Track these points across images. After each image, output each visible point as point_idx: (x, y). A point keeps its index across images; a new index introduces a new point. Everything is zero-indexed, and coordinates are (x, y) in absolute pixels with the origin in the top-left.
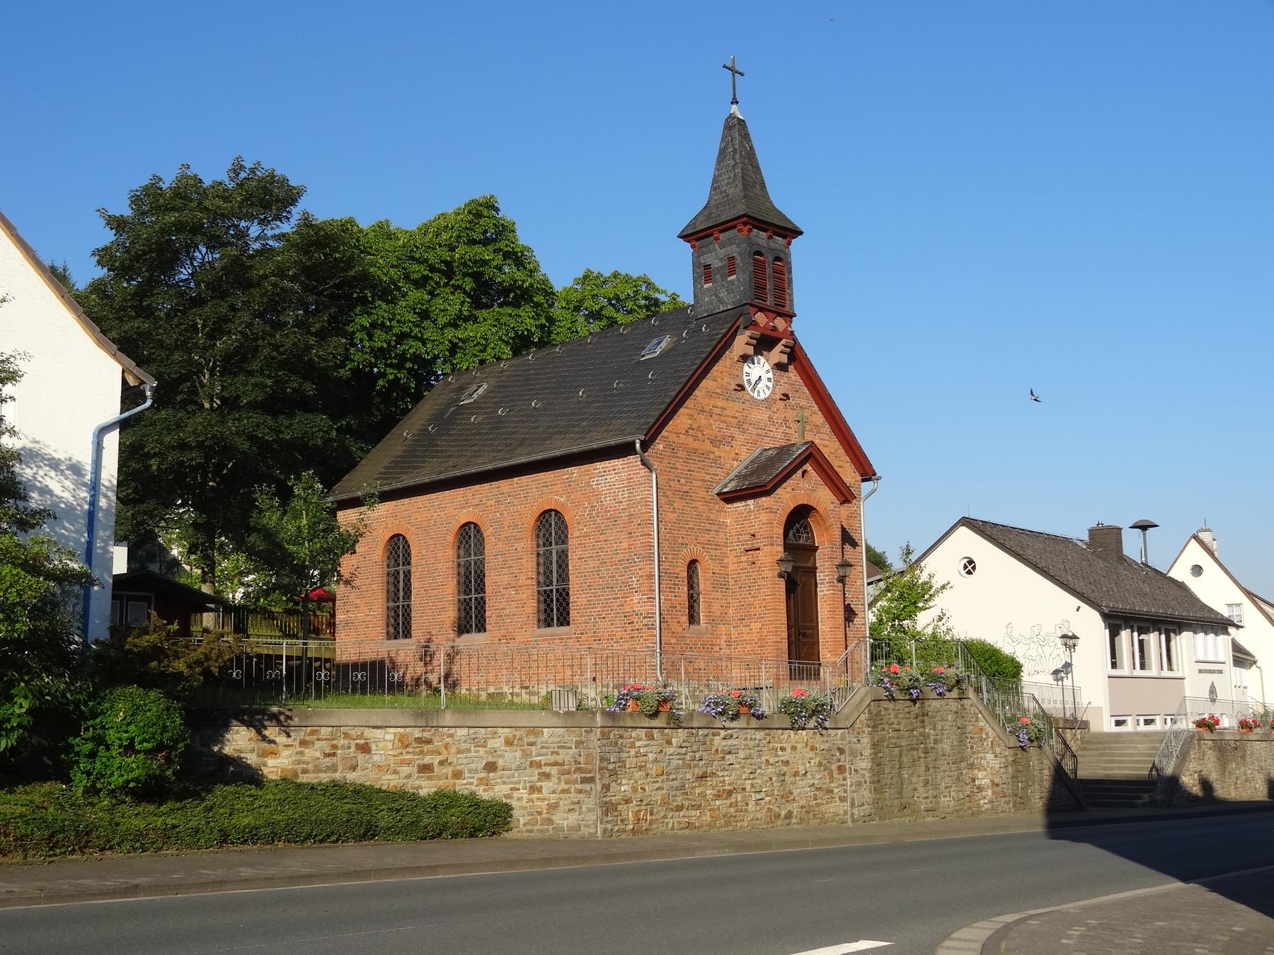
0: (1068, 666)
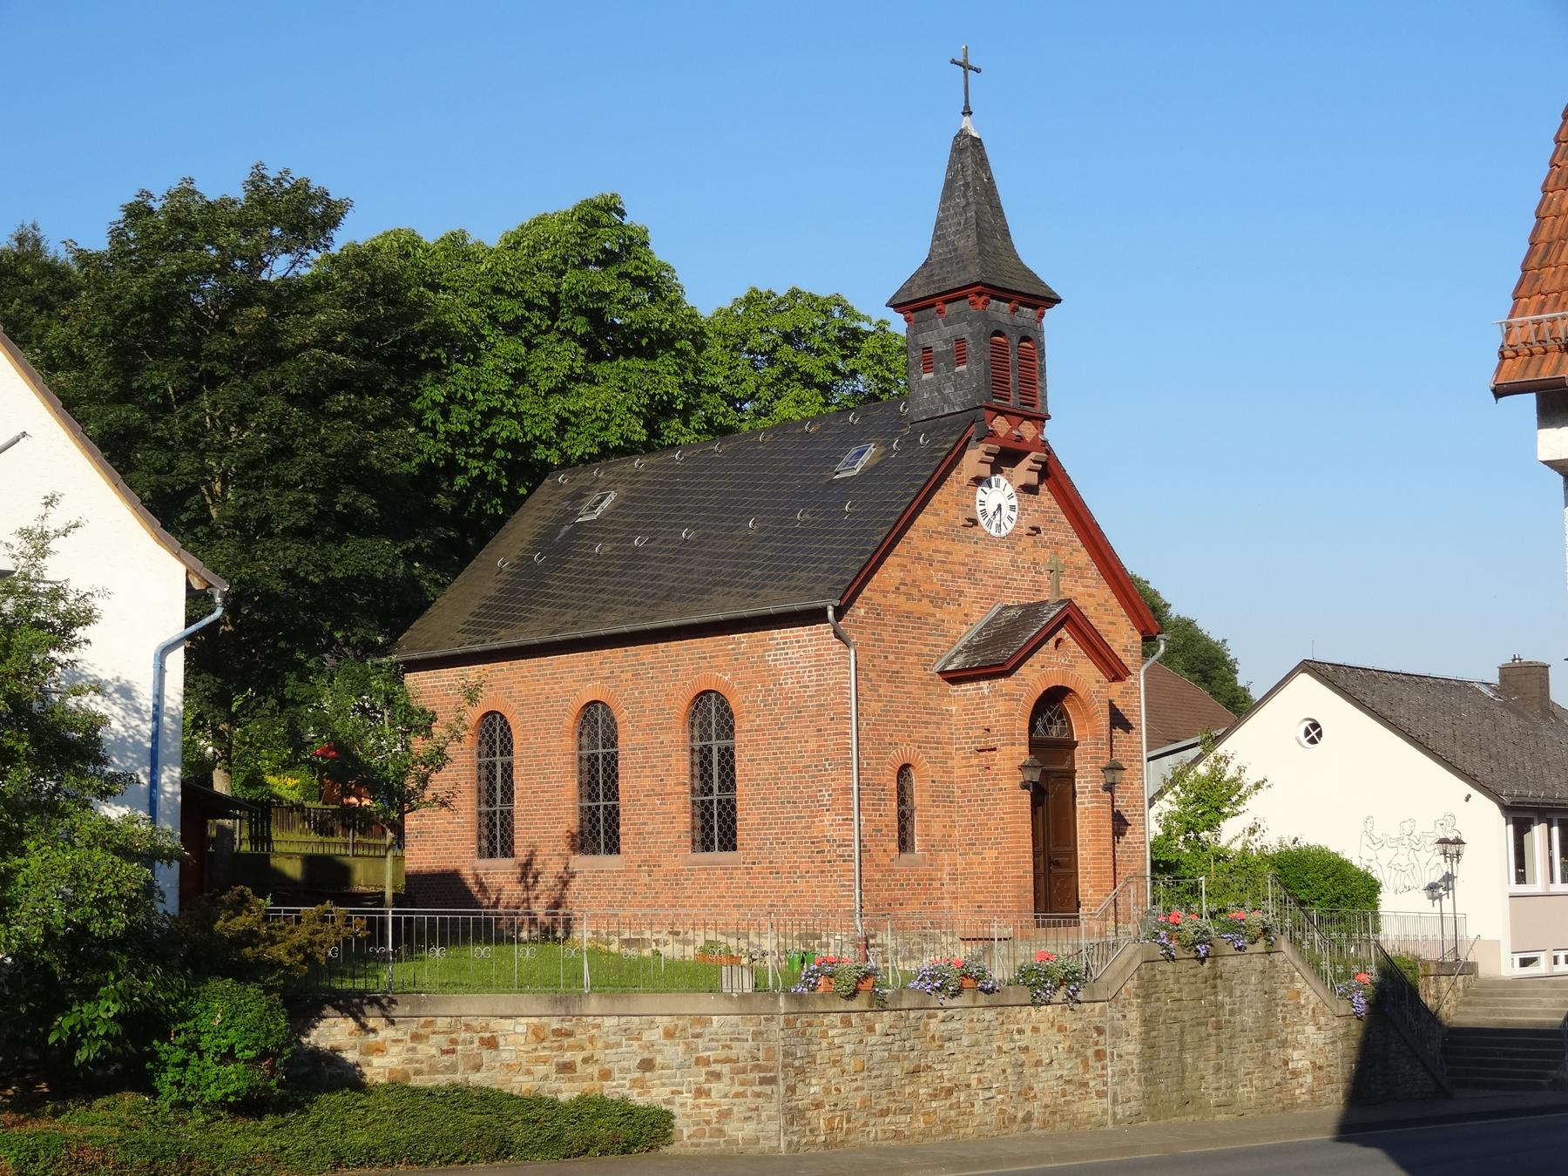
0: (1449, 878)
